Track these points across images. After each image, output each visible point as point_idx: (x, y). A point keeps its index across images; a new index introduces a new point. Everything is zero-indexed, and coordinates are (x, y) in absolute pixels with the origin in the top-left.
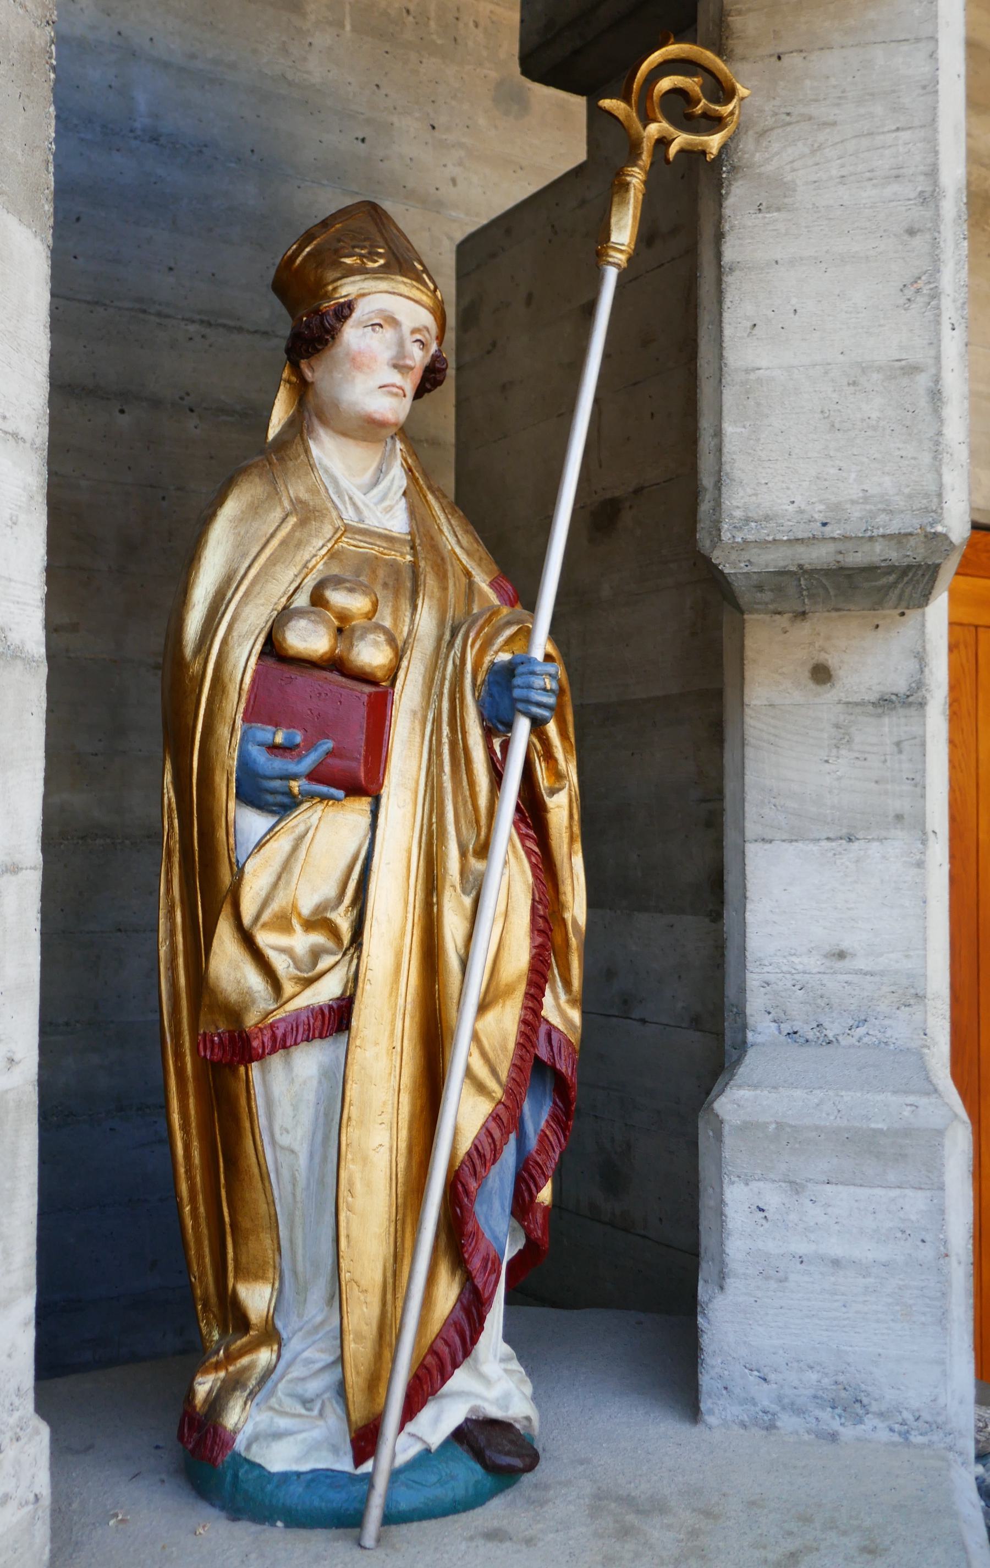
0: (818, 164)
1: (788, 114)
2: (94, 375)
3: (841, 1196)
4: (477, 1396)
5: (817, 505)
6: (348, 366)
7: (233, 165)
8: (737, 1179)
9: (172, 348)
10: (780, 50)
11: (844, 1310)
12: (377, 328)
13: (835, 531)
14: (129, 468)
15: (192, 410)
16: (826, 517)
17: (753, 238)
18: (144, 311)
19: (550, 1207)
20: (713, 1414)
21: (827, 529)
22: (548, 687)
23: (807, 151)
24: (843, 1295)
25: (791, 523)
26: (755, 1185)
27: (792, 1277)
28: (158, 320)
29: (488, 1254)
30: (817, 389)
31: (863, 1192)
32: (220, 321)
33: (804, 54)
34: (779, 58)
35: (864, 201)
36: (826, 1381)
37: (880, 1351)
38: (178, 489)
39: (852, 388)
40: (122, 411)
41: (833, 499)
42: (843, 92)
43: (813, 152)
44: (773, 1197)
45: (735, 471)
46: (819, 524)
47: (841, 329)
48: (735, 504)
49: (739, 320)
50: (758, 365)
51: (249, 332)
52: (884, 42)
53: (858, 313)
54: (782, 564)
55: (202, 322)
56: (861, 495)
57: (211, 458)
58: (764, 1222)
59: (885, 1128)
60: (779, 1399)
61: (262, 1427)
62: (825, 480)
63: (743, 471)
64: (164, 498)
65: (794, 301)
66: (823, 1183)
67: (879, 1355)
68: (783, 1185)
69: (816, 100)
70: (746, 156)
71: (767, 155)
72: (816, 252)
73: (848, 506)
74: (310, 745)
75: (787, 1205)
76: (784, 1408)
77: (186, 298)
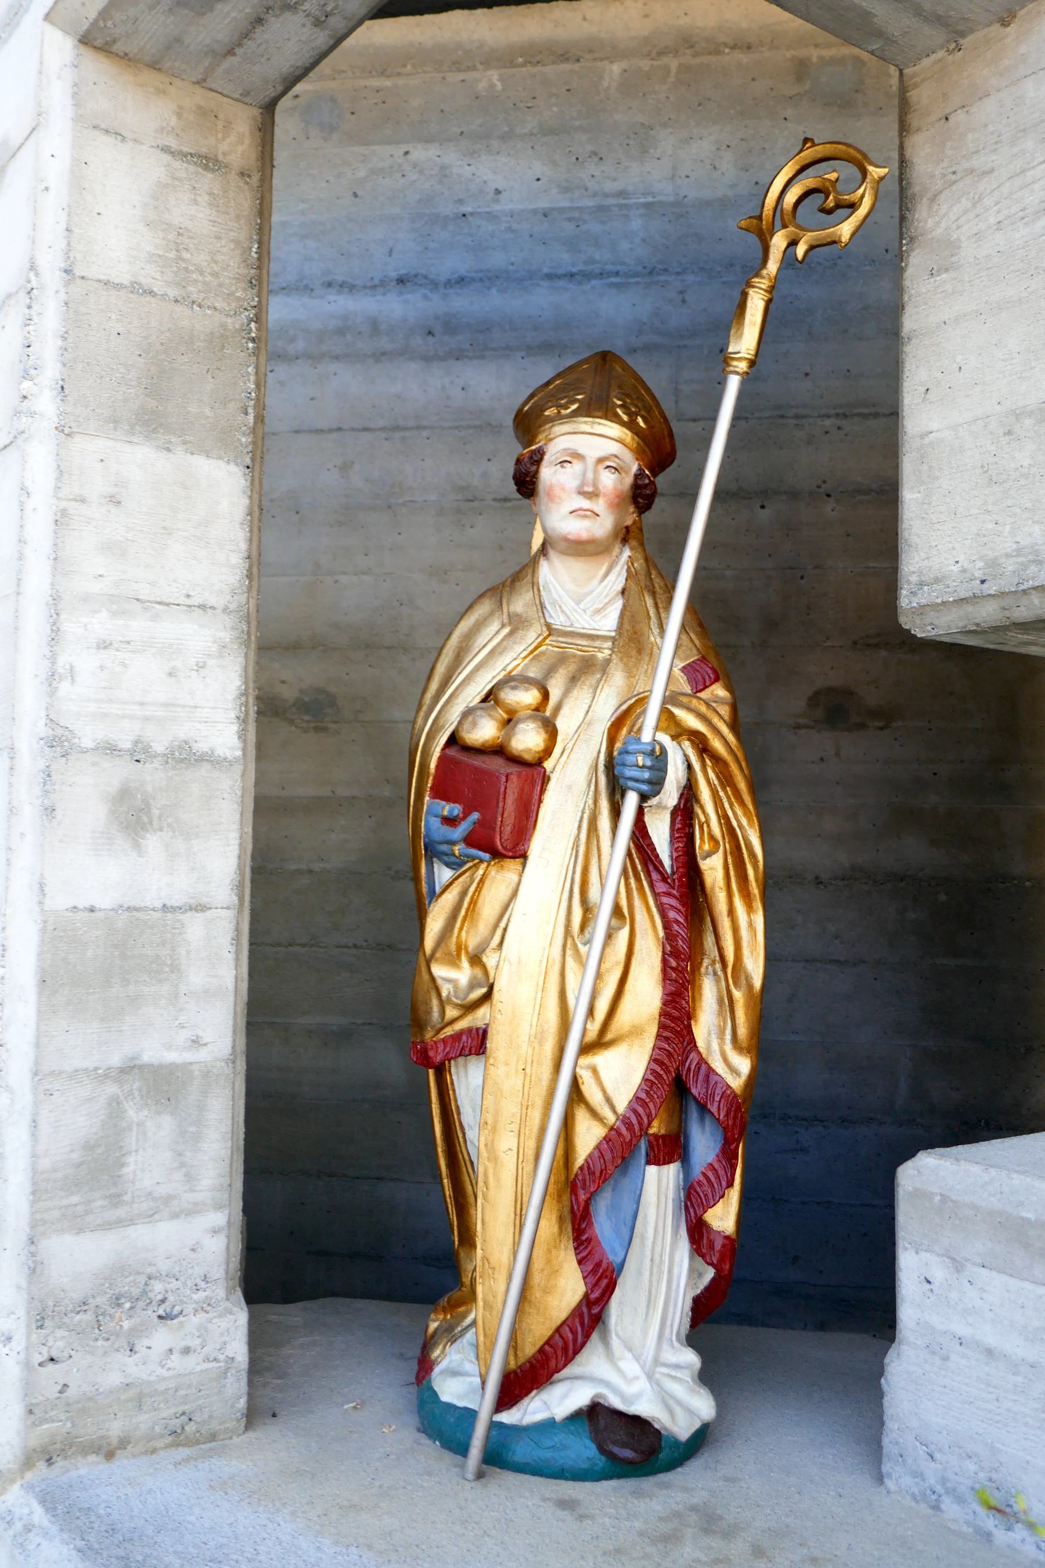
0: (978, 216)
1: (954, 173)
2: (737, 480)
3: (996, 1283)
4: (607, 1384)
5: (977, 562)
6: (546, 499)
7: (868, 268)
8: (909, 1246)
9: (808, 443)
10: (947, 111)
11: (996, 1404)
12: (565, 464)
13: (991, 588)
14: (770, 555)
15: (829, 496)
16: (984, 574)
17: (926, 304)
18: (782, 417)
19: (734, 1236)
20: (891, 1479)
21: (986, 585)
22: (641, 763)
23: (969, 205)
24: (995, 1388)
25: (956, 584)
26: (923, 1255)
27: (953, 1357)
28: (795, 421)
29: (601, 1261)
30: (978, 444)
31: (1013, 1283)
32: (856, 411)
33: (966, 109)
34: (947, 119)
35: (1018, 242)
36: (982, 1475)
37: (1028, 1458)
38: (816, 567)
39: (1007, 437)
40: (763, 507)
41: (990, 554)
42: (999, 136)
43: (974, 205)
44: (939, 1273)
45: (912, 537)
46: (978, 582)
47: (998, 378)
48: (912, 569)
49: (916, 387)
50: (930, 429)
51: (884, 415)
52: (1034, 73)
53: (1012, 359)
54: (961, 624)
55: (837, 415)
56: (1015, 546)
57: (848, 535)
58: (929, 1294)
59: (1033, 1219)
60: (944, 1481)
61: (454, 1365)
62: (984, 536)
63: (918, 536)
64: (802, 577)
65: (959, 358)
66: (978, 1265)
67: (1028, 1462)
68: (947, 1260)
69: (977, 152)
70: (921, 224)
71: (937, 219)
72: (977, 305)
73: (1003, 560)
74: (466, 814)
75: (950, 1282)
76: (947, 1493)
77: (822, 397)
